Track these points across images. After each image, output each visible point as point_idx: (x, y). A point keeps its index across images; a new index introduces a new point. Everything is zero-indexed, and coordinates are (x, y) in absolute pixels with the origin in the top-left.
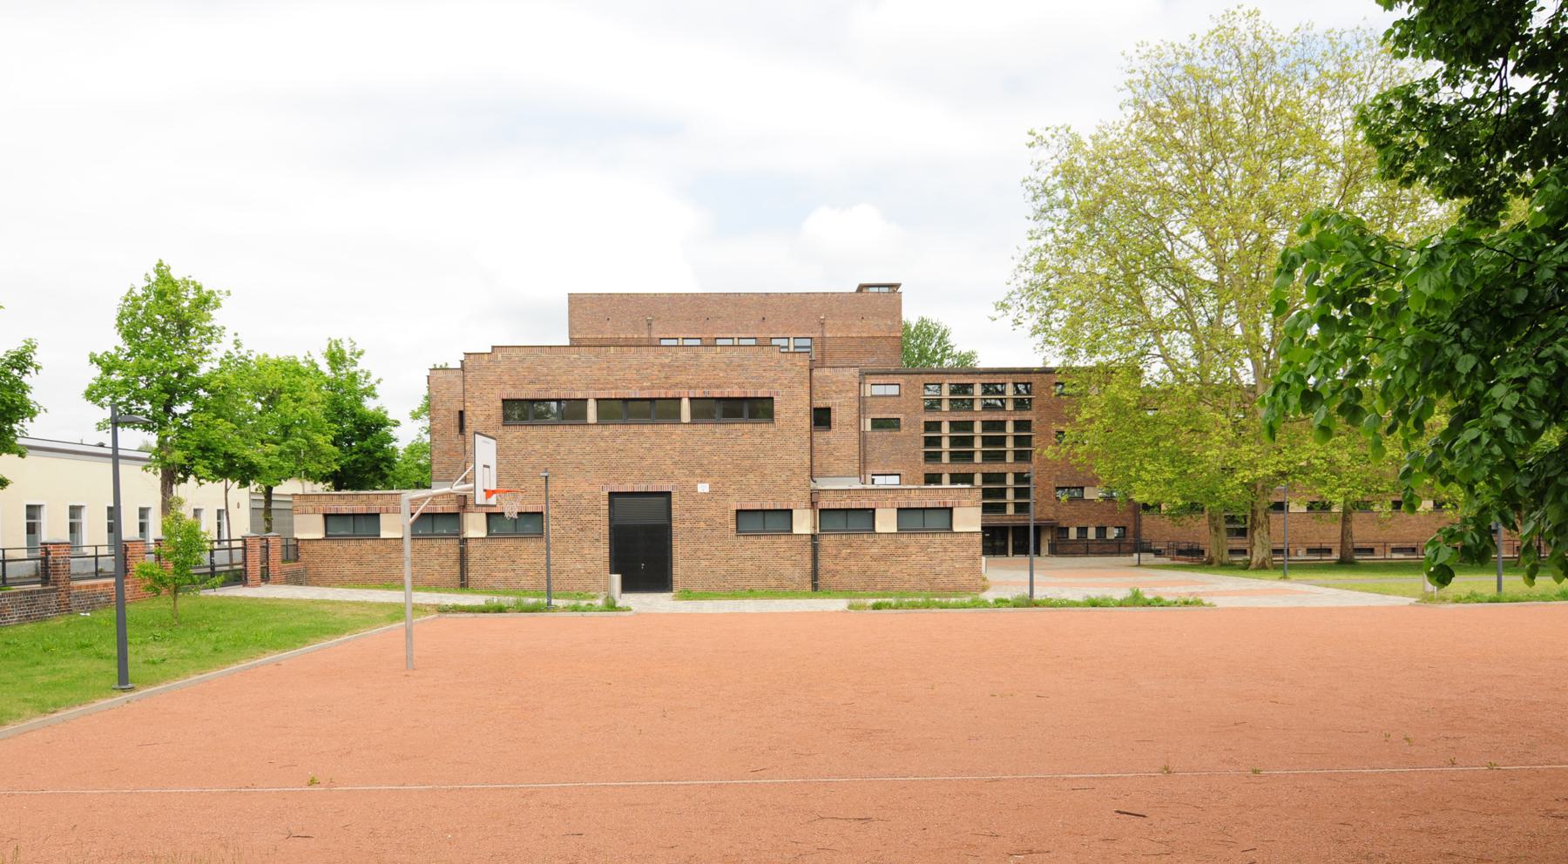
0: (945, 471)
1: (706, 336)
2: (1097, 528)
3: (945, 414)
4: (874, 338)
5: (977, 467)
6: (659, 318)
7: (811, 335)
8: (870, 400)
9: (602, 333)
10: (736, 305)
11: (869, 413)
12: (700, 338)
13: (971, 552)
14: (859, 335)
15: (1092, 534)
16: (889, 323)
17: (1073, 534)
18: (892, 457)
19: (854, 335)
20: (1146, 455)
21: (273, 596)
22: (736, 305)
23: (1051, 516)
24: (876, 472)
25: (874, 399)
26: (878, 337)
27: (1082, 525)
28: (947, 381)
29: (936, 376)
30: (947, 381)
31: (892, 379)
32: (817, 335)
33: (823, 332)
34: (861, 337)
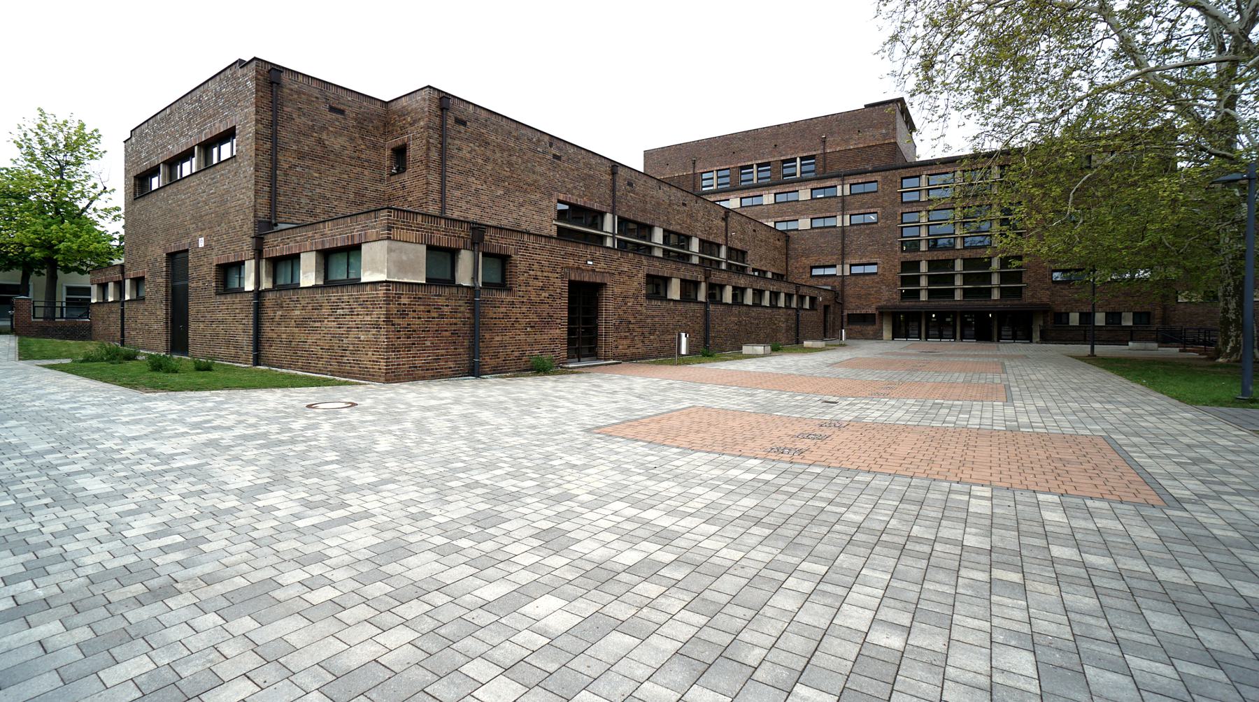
0: (922, 258)
2: (1107, 314)
3: (924, 204)
4: (869, 147)
5: (957, 253)
7: (814, 153)
9: (664, 175)
10: (755, 139)
12: (728, 169)
14: (856, 146)
15: (1100, 319)
17: (1074, 319)
18: (870, 248)
20: (965, 59)
22: (755, 139)
23: (1045, 300)
24: (854, 262)
26: (873, 146)
28: (925, 173)
29: (913, 169)
30: (925, 173)
31: (870, 177)
32: (819, 152)
33: (824, 149)
34: (858, 148)
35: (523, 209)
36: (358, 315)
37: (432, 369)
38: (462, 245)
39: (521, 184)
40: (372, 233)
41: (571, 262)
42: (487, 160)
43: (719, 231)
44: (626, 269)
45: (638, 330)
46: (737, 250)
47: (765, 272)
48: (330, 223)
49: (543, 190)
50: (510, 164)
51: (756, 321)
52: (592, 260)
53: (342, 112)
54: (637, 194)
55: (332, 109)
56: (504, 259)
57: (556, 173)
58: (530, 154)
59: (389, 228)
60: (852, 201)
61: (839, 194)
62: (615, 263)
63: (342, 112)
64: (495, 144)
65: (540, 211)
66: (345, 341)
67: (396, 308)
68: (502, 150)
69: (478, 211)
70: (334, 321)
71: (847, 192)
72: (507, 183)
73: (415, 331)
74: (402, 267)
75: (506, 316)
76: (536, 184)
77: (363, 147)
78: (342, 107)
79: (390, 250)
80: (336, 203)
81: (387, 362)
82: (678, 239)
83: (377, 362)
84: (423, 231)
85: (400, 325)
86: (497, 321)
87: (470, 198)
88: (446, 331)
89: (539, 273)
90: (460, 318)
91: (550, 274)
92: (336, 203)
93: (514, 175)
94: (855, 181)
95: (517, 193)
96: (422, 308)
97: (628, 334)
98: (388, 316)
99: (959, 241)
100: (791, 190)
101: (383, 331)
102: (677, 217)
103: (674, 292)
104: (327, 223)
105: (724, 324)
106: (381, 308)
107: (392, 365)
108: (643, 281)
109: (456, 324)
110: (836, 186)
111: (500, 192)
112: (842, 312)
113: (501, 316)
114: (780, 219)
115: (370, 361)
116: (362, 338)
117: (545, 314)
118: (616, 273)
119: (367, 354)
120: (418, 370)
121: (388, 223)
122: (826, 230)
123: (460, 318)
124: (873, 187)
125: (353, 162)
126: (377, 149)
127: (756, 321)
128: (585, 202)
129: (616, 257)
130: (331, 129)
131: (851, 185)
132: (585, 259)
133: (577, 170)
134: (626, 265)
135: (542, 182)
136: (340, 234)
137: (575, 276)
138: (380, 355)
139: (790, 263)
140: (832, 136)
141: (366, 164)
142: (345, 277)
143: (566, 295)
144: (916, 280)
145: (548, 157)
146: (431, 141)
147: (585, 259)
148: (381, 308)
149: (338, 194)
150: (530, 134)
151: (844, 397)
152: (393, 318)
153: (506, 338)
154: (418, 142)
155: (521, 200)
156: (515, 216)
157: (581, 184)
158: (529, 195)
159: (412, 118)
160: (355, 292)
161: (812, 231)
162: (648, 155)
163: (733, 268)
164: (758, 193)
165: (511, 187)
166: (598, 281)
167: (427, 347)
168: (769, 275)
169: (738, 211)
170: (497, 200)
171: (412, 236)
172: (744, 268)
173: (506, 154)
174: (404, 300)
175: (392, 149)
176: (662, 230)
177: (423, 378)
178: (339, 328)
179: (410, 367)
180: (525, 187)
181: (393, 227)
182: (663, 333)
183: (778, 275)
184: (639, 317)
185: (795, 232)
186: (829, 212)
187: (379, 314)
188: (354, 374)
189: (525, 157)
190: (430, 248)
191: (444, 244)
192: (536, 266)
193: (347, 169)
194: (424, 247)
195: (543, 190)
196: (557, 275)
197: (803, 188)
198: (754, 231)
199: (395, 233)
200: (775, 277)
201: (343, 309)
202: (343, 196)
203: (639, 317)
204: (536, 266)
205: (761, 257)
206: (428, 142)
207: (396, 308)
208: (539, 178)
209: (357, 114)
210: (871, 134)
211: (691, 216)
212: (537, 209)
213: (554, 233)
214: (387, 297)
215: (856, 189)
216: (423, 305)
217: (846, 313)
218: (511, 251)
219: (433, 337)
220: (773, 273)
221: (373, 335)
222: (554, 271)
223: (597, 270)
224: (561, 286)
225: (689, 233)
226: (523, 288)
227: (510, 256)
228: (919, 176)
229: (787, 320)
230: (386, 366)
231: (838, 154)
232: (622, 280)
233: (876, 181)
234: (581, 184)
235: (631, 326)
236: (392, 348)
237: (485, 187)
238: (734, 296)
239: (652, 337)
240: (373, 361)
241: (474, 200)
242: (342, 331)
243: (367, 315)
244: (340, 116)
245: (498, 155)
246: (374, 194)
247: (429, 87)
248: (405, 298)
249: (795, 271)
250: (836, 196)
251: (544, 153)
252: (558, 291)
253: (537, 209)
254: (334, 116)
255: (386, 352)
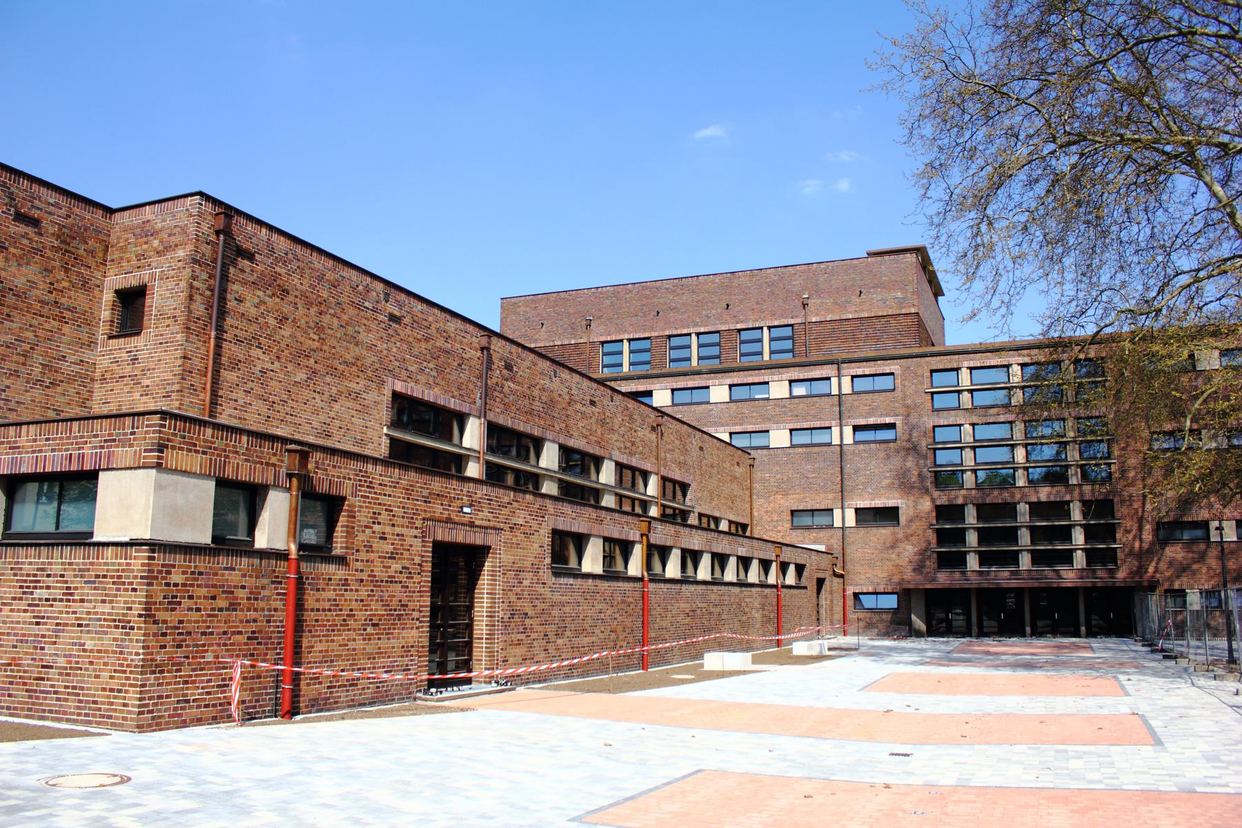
0: (549, 435)
1: (656, 334)
6: (600, 317)
7: (791, 321)
8: (850, 398)
9: (536, 341)
11: (849, 417)
12: (649, 338)
13: (119, 608)
16: (899, 295)
19: (850, 316)
21: (1017, 673)
25: (855, 397)
27: (243, 472)
32: (798, 320)
35: (337, 406)
36: (82, 601)
37: (214, 705)
38: (271, 481)
39: (336, 363)
40: (123, 454)
41: (438, 510)
42: (283, 320)
43: (647, 449)
44: (521, 521)
45: (540, 628)
46: (674, 482)
47: (717, 520)
48: (32, 427)
49: (370, 373)
50: (319, 329)
51: (718, 610)
52: (471, 506)
53: (35, 222)
54: (519, 384)
55: (20, 217)
56: (332, 506)
57: (391, 345)
58: (352, 311)
59: (161, 448)
60: (856, 403)
61: (835, 391)
62: (505, 511)
63: (35, 222)
64: (297, 293)
65: (364, 410)
66: (49, 649)
67: (162, 591)
68: (309, 305)
69: (259, 406)
70: (25, 611)
71: (847, 389)
72: (312, 361)
73: (189, 633)
74: (165, 511)
75: (336, 606)
76: (359, 363)
77: (66, 284)
78: (36, 214)
79: (159, 487)
80: (7, 382)
81: (141, 692)
82: (630, 474)
83: (120, 691)
84: (213, 454)
85: (165, 622)
86: (321, 616)
87: (250, 385)
88: (240, 633)
89: (388, 529)
90: (263, 610)
91: (404, 531)
92: (7, 382)
93: (325, 348)
94: (860, 372)
95: (328, 379)
96: (204, 591)
97: (522, 636)
98: (148, 607)
99: (1020, 473)
100: (756, 380)
101: (137, 635)
102: (580, 424)
103: (592, 562)
104: (24, 428)
105: (669, 615)
106: (134, 590)
107: (150, 698)
108: (547, 541)
109: (255, 621)
110: (829, 379)
111: (301, 376)
112: (844, 590)
113: (327, 605)
114: (738, 429)
115: (104, 689)
116: (89, 645)
117: (395, 602)
118: (506, 527)
119: (97, 677)
120: (191, 707)
121: (160, 438)
122: (816, 449)
123: (263, 610)
124: (886, 383)
125: (45, 311)
126: (89, 290)
127: (718, 610)
128: (436, 397)
129: (506, 500)
130: (12, 250)
131: (853, 377)
132: (459, 503)
133: (427, 340)
134: (522, 514)
135: (370, 359)
136: (53, 450)
137: (443, 533)
138: (128, 678)
139: (755, 506)
140: (819, 297)
141: (67, 314)
142: (52, 529)
143: (428, 567)
144: (959, 536)
145: (381, 318)
146: (195, 283)
147: (459, 503)
148: (134, 590)
149: (13, 366)
150: (354, 278)
151: (924, 741)
152: (158, 610)
153: (334, 646)
154: (171, 284)
155: (334, 390)
156: (323, 417)
157: (431, 365)
158: (346, 383)
159: (161, 242)
160: (77, 557)
161: (791, 451)
162: (508, 305)
163: (510, 480)
164: (703, 384)
165: (317, 367)
166: (479, 542)
167: (209, 663)
168: (724, 526)
169: (669, 411)
170: (294, 389)
171: (195, 462)
172: (684, 514)
173: (314, 310)
174: (176, 577)
175: (117, 292)
176: (557, 446)
177: (199, 721)
178: (38, 623)
179: (178, 702)
180: (341, 367)
181: (167, 447)
182: (578, 633)
183: (737, 524)
184: (540, 606)
185: (765, 452)
186: (820, 419)
187: (132, 602)
188: (65, 713)
189: (345, 317)
190: (222, 483)
191: (244, 476)
192: (384, 517)
193: (35, 322)
194: (211, 485)
195: (370, 373)
196: (416, 532)
197: (776, 378)
198: (701, 448)
199: (172, 459)
200: (733, 530)
201: (48, 588)
202: (22, 368)
203: (540, 606)
204: (384, 517)
205: (711, 492)
206: (191, 286)
207: (162, 591)
208: (364, 352)
209: (61, 227)
210: (880, 298)
211: (603, 423)
212: (359, 408)
213: (383, 450)
214: (150, 571)
215: (862, 384)
216: (207, 586)
217: (850, 591)
218: (346, 490)
219: (219, 645)
220: (730, 522)
221: (115, 640)
222: (412, 525)
223: (477, 523)
224: (419, 551)
225: (598, 451)
226: (363, 555)
227: (344, 499)
228: (957, 370)
229: (763, 606)
230: (140, 699)
231: (829, 326)
232: (514, 540)
233: (892, 374)
234: (431, 365)
235: (528, 621)
236: (151, 666)
237: (277, 365)
238: (608, 559)
239: (560, 641)
240: (112, 690)
241: (258, 390)
242: (42, 630)
243: (103, 601)
244: (30, 231)
245: (302, 311)
246: (76, 368)
247: (201, 194)
248: (176, 573)
249: (765, 517)
250: (829, 395)
251: (374, 310)
252: (417, 560)
253: (359, 408)
254: (22, 229)
255: (142, 673)
